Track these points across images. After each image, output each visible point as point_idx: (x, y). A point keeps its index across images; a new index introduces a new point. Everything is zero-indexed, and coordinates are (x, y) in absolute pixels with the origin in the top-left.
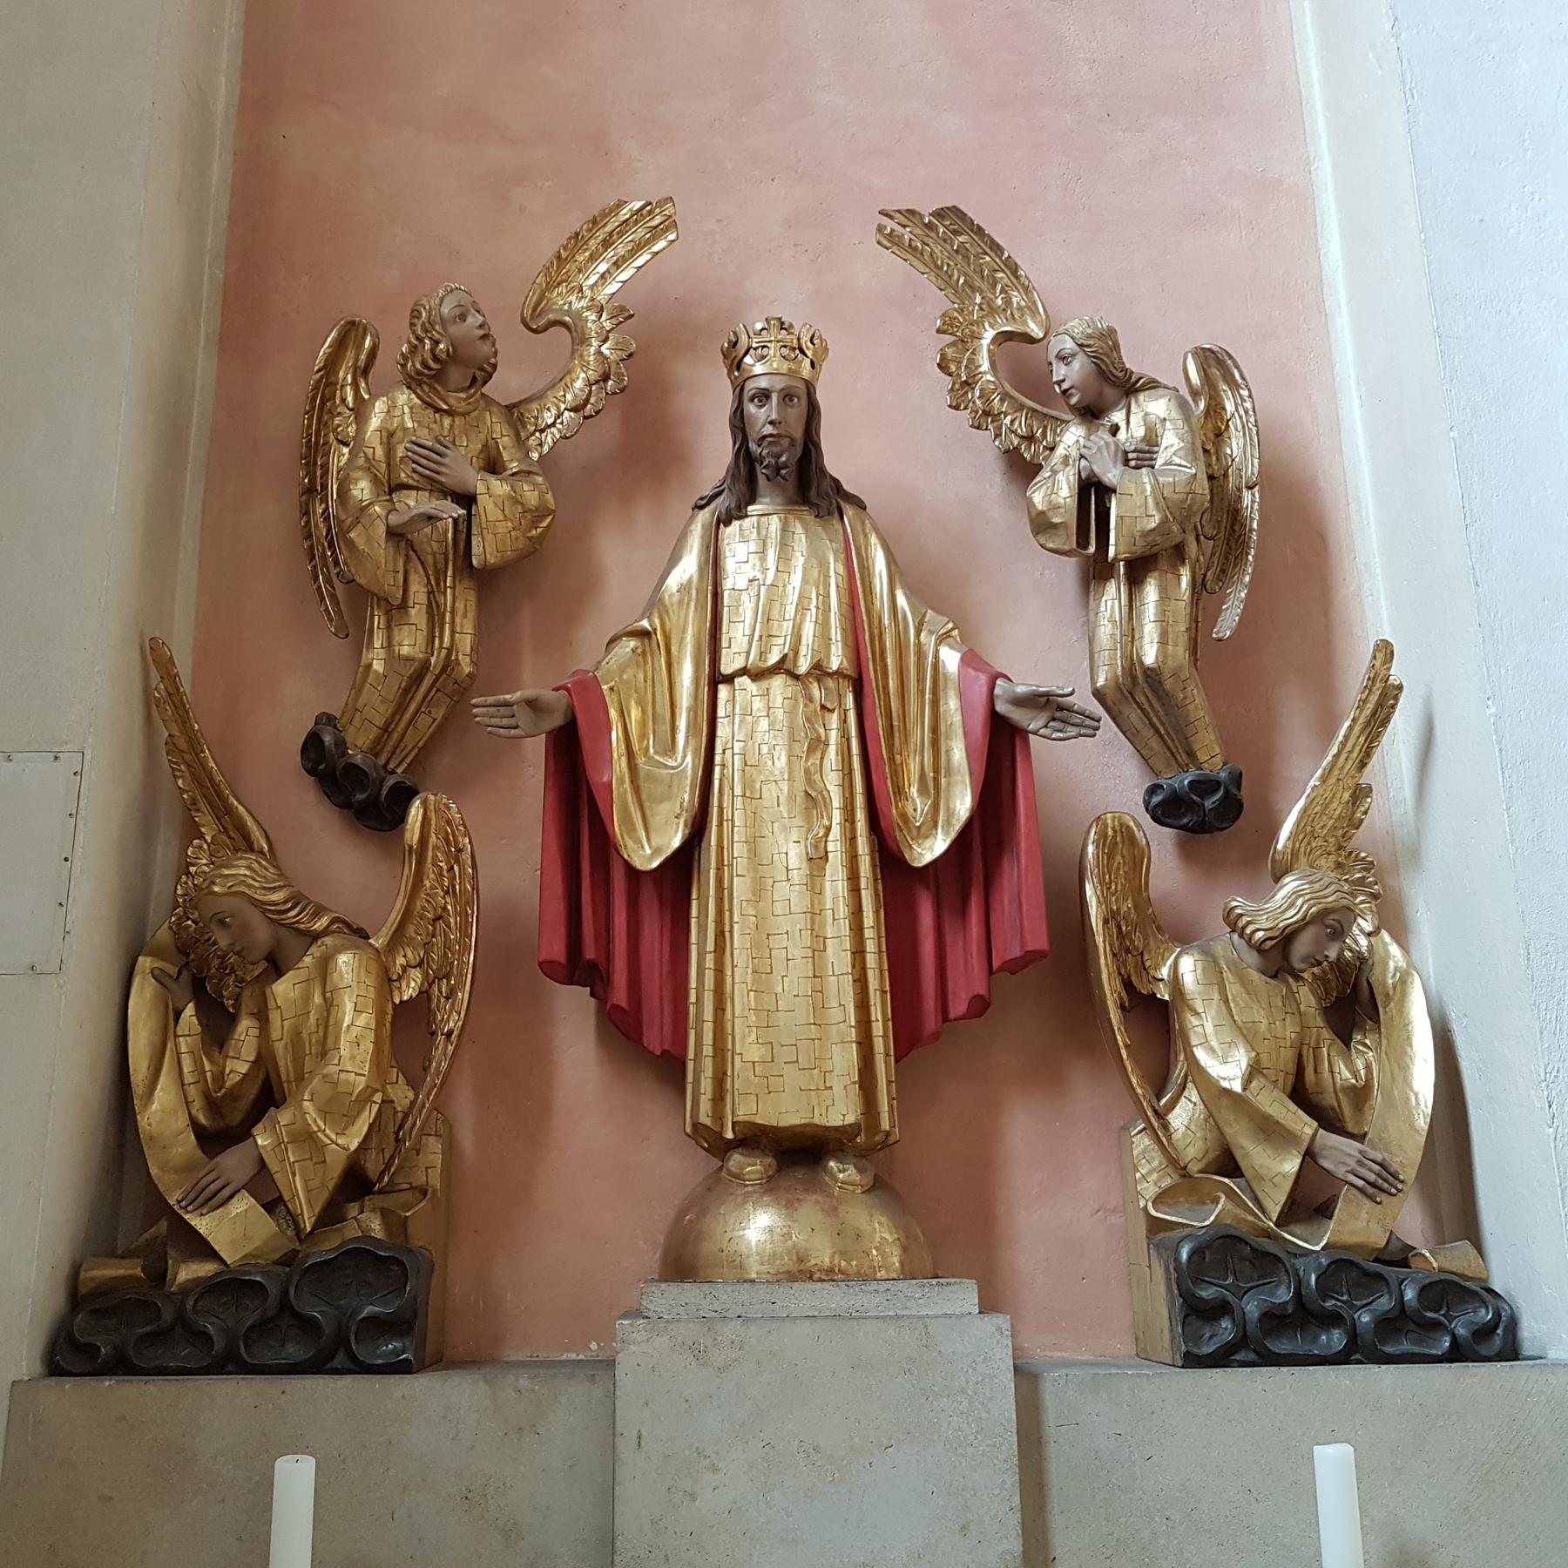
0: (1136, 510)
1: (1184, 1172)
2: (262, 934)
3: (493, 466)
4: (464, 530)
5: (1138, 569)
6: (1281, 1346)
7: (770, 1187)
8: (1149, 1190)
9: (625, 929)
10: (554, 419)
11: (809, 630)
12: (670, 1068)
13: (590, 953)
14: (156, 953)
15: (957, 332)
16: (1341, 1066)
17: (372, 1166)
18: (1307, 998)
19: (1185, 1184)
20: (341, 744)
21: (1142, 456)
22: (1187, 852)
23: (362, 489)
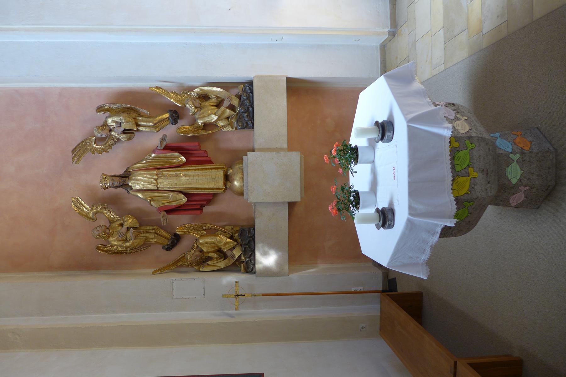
0: (130, 126)
1: (229, 124)
2: (197, 253)
3: (122, 225)
4: (134, 228)
5: (138, 125)
6: (251, 115)
7: (232, 182)
8: (231, 129)
9: (196, 202)
10: (113, 216)
11: (150, 176)
12: (214, 195)
13: (199, 207)
14: (199, 268)
15: (94, 151)
16: (214, 100)
17: (229, 236)
18: (204, 104)
19: (230, 124)
20: (168, 245)
21: (119, 124)
22: (182, 118)
23: (128, 244)
